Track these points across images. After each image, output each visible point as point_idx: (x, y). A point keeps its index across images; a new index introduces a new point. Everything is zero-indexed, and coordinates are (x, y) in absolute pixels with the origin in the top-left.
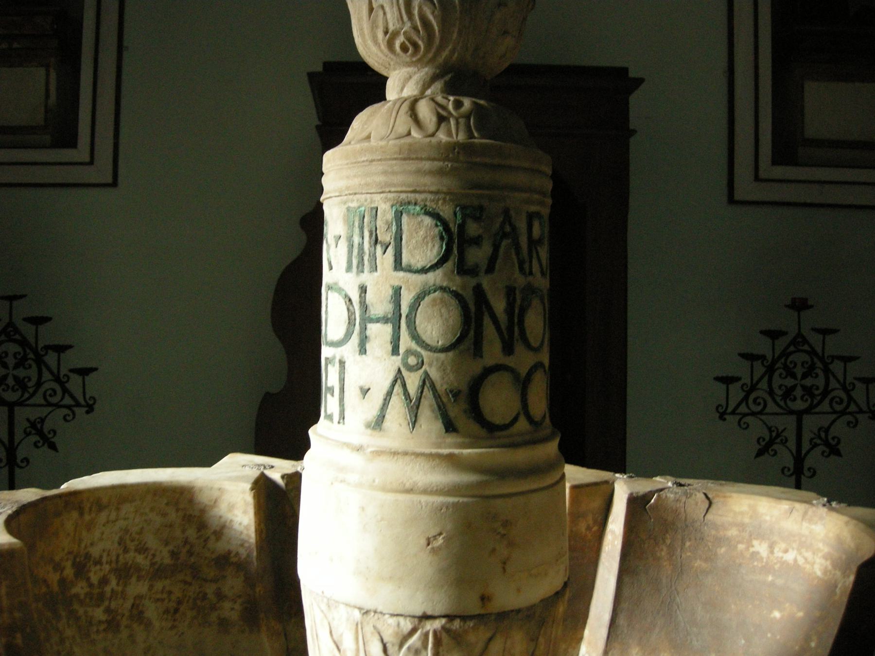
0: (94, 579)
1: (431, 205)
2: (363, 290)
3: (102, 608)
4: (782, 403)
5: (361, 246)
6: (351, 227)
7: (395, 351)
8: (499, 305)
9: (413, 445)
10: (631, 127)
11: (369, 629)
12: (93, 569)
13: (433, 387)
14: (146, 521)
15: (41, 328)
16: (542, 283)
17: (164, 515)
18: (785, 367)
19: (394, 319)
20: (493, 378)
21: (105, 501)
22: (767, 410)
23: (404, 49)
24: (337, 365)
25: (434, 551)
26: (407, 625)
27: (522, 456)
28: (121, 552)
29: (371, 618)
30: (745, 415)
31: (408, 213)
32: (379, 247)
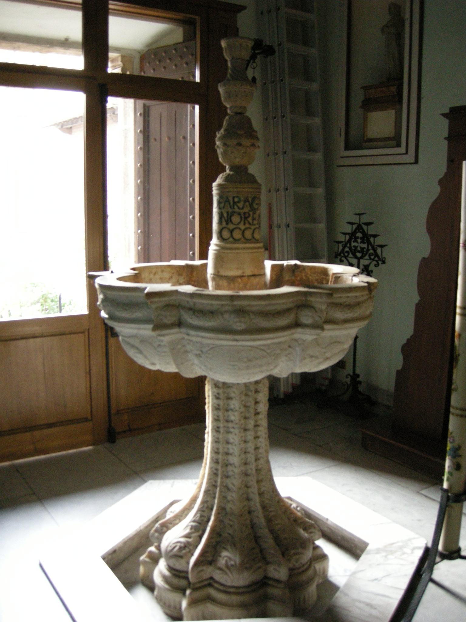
8: (225, 215)
10: (445, 123)
15: (369, 227)
20: (255, 231)
27: (228, 245)
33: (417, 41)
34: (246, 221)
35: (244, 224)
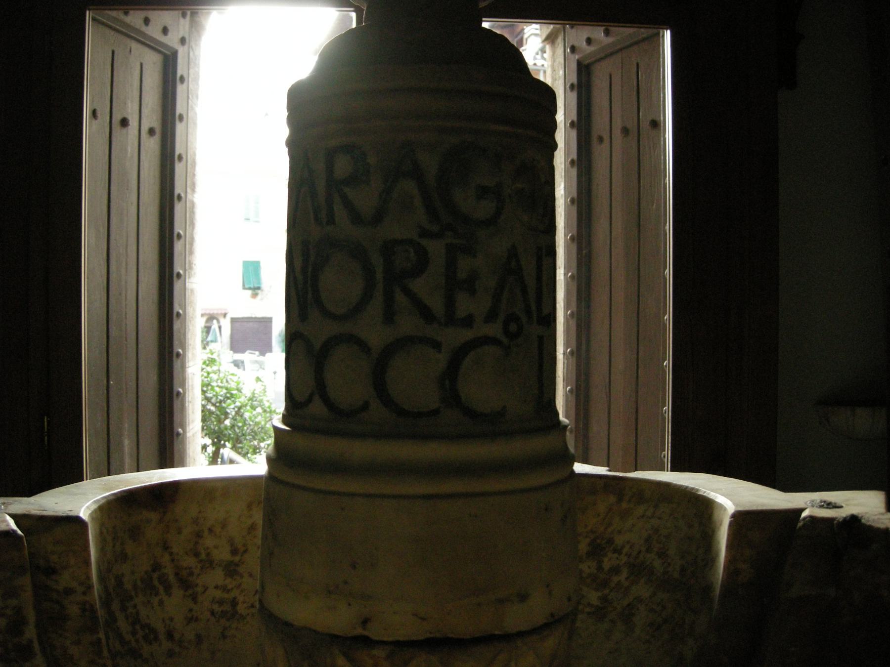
0: (606, 565)
3: (600, 594)
12: (610, 555)
28: (643, 549)
33: (595, 109)
34: (400, 298)
35: (389, 316)
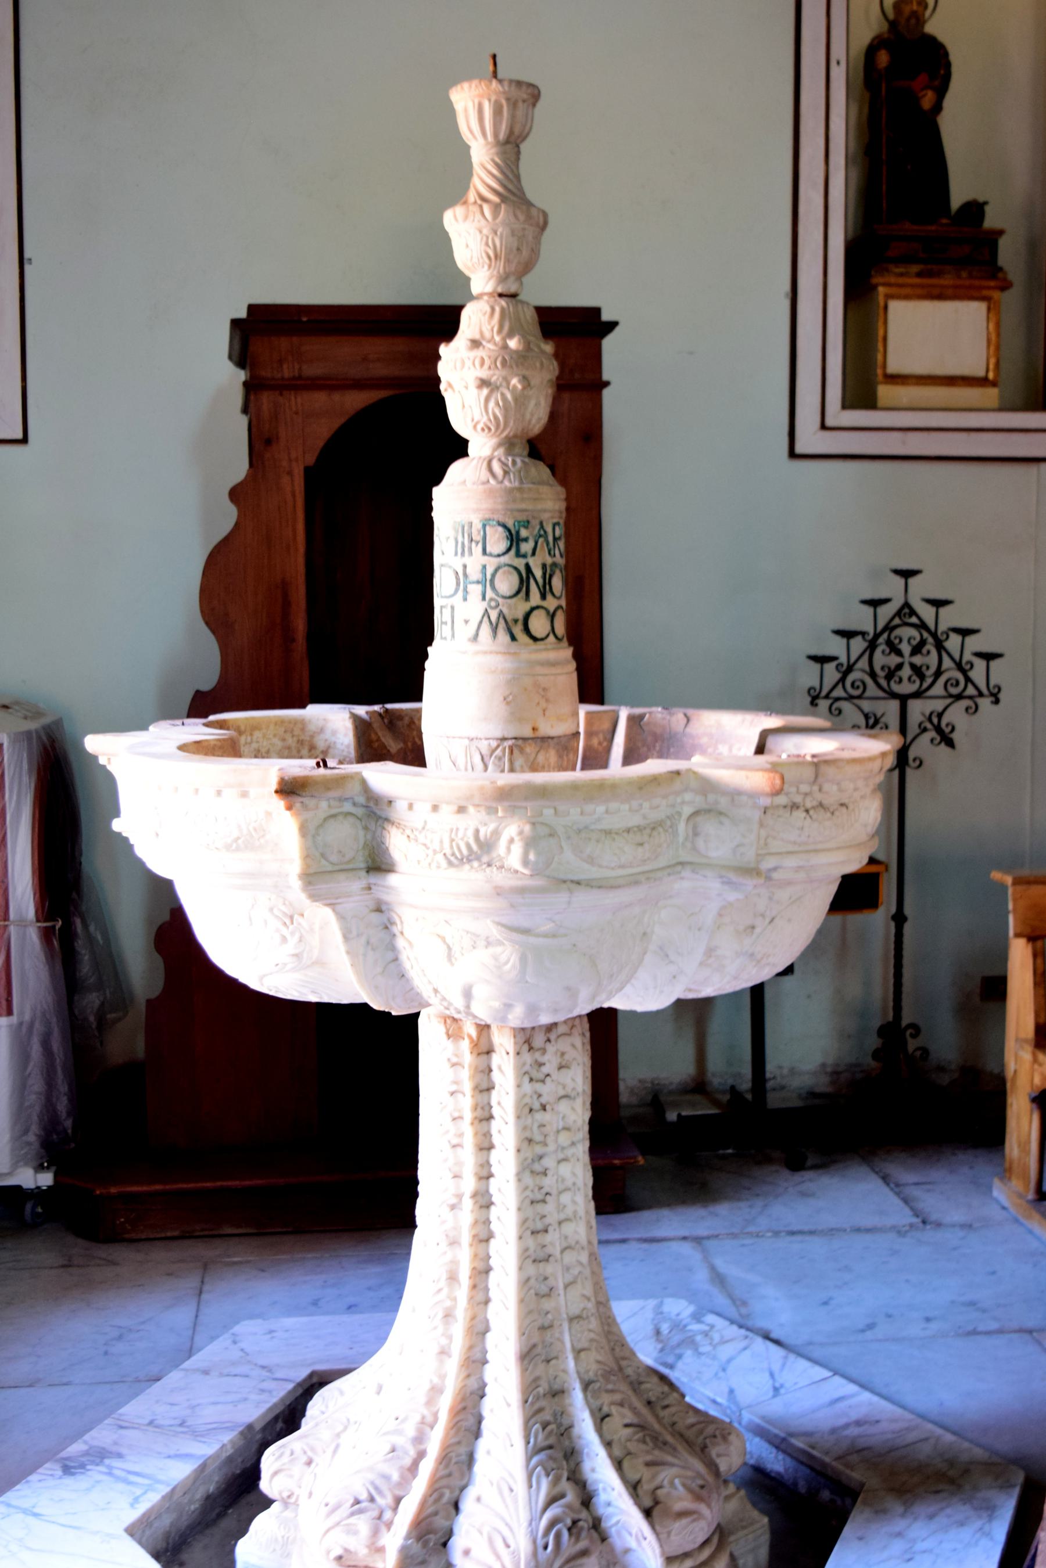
1: (501, 519)
2: (465, 567)
4: (883, 683)
5: (463, 544)
6: (457, 532)
7: (484, 598)
8: (538, 573)
9: (494, 648)
11: (473, 748)
13: (504, 618)
14: (270, 744)
16: (561, 561)
17: (284, 740)
18: (889, 643)
19: (482, 582)
20: (535, 613)
21: (243, 728)
22: (867, 694)
23: (483, 430)
24: (449, 609)
25: (508, 703)
26: (494, 744)
29: (475, 742)
30: (837, 699)
31: (490, 525)
32: (474, 544)
